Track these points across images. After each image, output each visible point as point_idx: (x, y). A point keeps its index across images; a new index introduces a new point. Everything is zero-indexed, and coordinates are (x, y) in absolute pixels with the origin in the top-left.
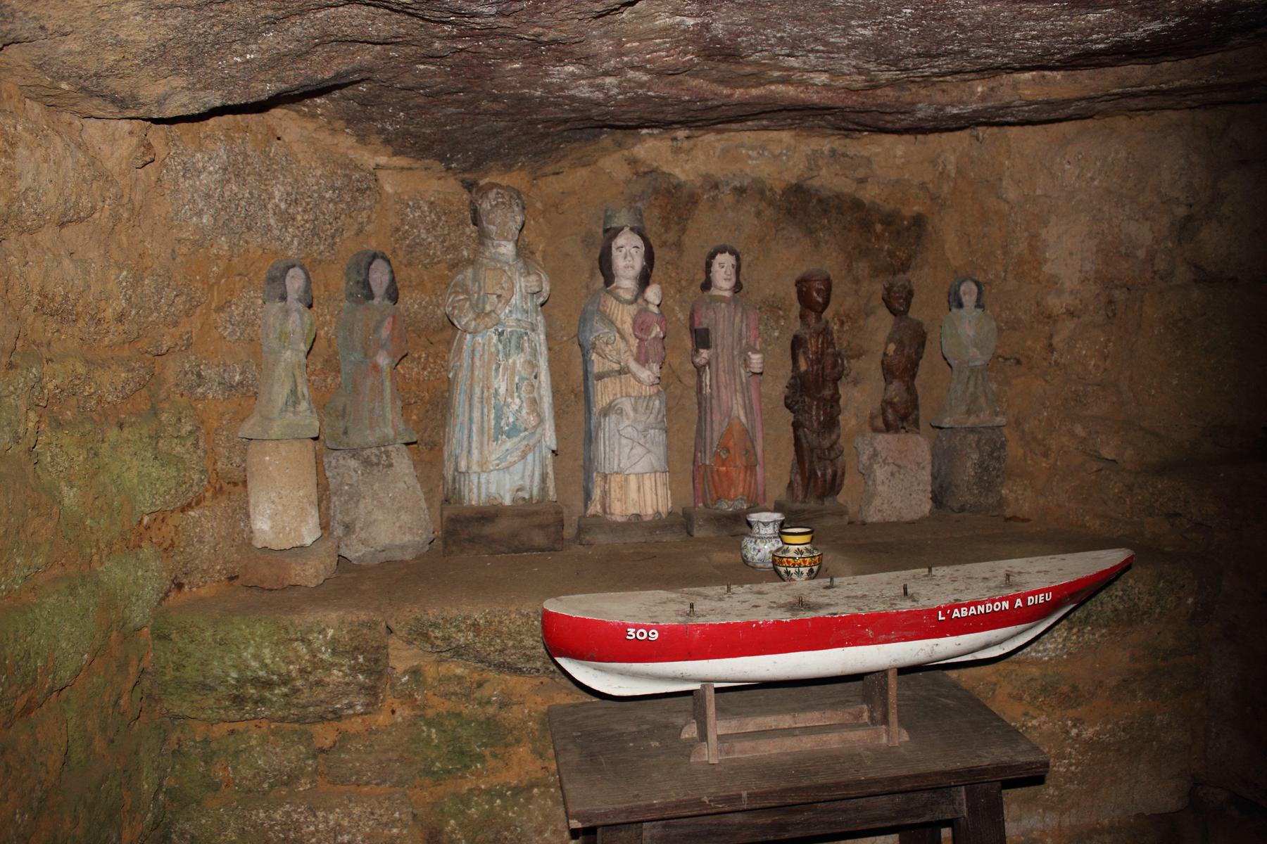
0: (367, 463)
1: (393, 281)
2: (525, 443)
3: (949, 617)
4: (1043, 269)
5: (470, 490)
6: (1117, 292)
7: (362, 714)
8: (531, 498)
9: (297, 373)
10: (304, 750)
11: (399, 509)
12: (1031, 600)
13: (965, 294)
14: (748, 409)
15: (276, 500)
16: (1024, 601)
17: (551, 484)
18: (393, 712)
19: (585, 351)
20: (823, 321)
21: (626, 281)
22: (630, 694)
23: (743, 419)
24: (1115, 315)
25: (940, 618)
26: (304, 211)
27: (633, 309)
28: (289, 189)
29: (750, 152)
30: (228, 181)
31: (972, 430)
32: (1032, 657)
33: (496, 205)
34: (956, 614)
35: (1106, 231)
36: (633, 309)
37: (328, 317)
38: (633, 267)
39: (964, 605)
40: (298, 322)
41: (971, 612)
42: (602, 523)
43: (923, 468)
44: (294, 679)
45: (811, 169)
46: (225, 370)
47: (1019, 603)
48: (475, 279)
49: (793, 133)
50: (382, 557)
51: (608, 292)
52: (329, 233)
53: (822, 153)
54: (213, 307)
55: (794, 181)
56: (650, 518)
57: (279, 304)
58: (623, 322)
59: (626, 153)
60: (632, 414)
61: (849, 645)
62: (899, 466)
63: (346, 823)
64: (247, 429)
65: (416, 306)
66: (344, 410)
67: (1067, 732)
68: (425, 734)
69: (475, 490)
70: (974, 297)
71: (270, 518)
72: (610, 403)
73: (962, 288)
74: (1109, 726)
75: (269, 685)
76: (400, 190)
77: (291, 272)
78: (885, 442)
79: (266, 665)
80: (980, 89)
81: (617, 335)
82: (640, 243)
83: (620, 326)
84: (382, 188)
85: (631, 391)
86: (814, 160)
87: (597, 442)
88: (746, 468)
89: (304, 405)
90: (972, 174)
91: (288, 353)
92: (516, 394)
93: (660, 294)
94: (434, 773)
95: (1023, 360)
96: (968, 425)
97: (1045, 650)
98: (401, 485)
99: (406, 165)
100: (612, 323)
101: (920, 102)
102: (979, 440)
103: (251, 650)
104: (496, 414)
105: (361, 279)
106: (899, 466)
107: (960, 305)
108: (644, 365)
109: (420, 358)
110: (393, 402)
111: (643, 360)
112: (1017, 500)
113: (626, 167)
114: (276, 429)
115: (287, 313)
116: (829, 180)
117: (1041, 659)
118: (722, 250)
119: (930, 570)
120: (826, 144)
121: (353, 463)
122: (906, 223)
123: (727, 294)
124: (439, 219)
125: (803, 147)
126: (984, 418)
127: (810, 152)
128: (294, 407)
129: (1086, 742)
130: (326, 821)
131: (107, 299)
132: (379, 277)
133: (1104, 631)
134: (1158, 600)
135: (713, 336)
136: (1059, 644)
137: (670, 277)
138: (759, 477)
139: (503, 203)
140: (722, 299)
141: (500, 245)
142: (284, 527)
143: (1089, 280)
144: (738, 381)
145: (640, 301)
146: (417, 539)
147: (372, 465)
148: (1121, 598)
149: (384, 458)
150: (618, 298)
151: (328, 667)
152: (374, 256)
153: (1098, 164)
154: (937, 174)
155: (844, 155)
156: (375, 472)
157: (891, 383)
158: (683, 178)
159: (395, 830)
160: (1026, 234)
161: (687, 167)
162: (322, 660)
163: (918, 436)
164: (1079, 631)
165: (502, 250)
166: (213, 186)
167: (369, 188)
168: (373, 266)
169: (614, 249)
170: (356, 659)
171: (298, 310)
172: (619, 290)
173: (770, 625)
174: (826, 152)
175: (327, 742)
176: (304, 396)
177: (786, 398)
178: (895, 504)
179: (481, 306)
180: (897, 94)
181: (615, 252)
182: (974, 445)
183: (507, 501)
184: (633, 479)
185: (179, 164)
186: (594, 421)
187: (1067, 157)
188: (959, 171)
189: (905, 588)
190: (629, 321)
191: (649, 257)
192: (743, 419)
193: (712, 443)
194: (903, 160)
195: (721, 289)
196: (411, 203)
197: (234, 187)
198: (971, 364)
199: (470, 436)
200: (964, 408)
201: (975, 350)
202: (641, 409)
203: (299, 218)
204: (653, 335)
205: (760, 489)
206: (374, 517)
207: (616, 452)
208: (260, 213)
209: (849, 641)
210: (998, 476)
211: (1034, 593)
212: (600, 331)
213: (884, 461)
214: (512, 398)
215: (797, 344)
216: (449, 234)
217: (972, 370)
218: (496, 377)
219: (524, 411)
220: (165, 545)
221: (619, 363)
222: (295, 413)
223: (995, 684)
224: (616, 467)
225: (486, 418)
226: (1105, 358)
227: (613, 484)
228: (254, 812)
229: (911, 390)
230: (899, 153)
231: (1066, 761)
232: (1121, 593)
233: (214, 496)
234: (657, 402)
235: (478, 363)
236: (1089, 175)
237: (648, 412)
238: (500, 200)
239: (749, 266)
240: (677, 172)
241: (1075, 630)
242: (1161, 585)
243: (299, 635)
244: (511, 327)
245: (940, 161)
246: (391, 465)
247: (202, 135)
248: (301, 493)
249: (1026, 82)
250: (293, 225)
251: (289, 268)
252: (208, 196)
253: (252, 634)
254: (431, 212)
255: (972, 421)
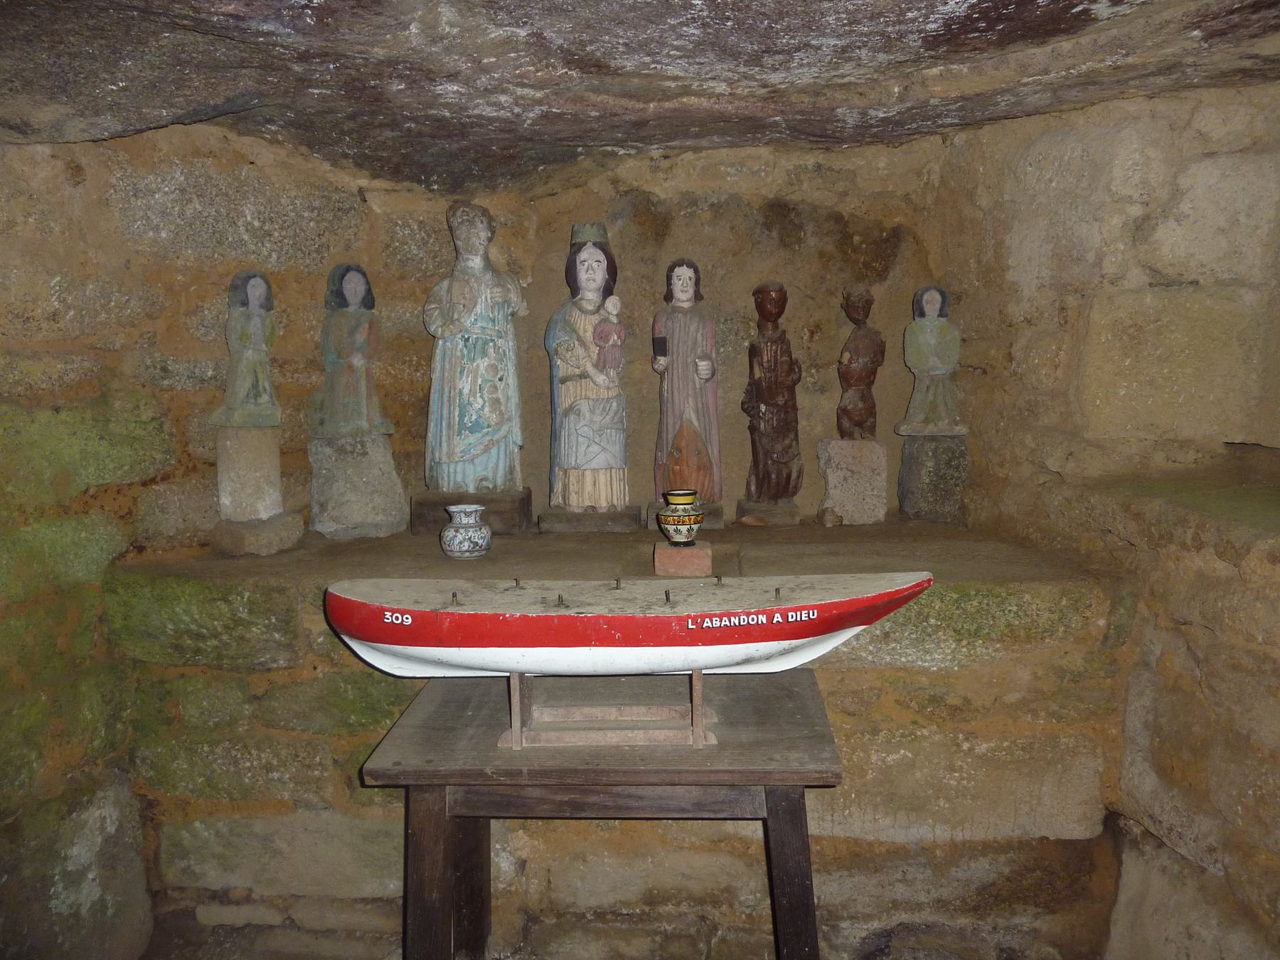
0: (341, 450)
1: (369, 291)
2: (489, 438)
3: (700, 626)
4: (1006, 276)
5: (442, 479)
6: (1071, 298)
7: (286, 668)
8: (495, 487)
9: (259, 370)
10: (241, 696)
11: (373, 493)
12: (792, 617)
13: (927, 303)
14: (702, 412)
15: (235, 479)
16: (785, 617)
17: (518, 475)
18: (315, 668)
19: (550, 356)
20: (780, 330)
21: (590, 295)
22: (391, 672)
23: (696, 423)
24: (1066, 322)
25: (690, 626)
26: (282, 228)
27: (595, 319)
28: (262, 208)
29: (729, 169)
30: (190, 201)
31: (933, 438)
32: (920, 666)
33: (462, 222)
34: (707, 623)
35: (1060, 234)
36: (595, 319)
37: (314, 322)
38: (594, 280)
39: (716, 615)
40: (259, 325)
41: (723, 623)
42: (562, 514)
43: (879, 474)
44: (220, 634)
45: (792, 185)
46: (195, 367)
47: (778, 618)
48: (449, 291)
49: (771, 149)
50: (356, 534)
51: (574, 304)
52: (313, 248)
53: (806, 168)
54: (182, 311)
55: (771, 196)
56: (605, 511)
57: (241, 309)
58: (585, 331)
59: (610, 173)
60: (588, 415)
61: (595, 646)
62: (852, 471)
63: (275, 762)
64: (217, 416)
65: (408, 315)
66: (322, 404)
67: (958, 745)
68: (342, 690)
69: (446, 479)
70: (938, 306)
71: (231, 494)
72: (572, 404)
73: (925, 297)
74: (1005, 744)
75: (199, 637)
76: (389, 211)
77: (252, 282)
78: (838, 448)
79: (196, 620)
80: (896, 90)
81: (576, 343)
82: (602, 257)
83: (582, 334)
84: (371, 209)
85: (589, 394)
86: (796, 176)
87: (560, 440)
88: (699, 468)
89: (265, 398)
90: (953, 183)
91: (250, 352)
92: (478, 395)
93: (619, 306)
94: (351, 725)
95: (988, 369)
96: (926, 433)
97: (933, 660)
98: (376, 472)
99: (388, 188)
100: (575, 331)
101: (838, 107)
102: (937, 447)
103: (183, 606)
104: (460, 411)
105: (335, 289)
106: (852, 471)
107: (922, 315)
108: (602, 372)
109: (411, 361)
110: (369, 396)
111: (601, 366)
112: (976, 510)
113: (610, 187)
114: (237, 417)
115: (248, 317)
116: (810, 193)
117: (929, 668)
118: (680, 263)
119: (719, 579)
120: (810, 160)
121: (328, 450)
122: (885, 234)
123: (686, 305)
124: (429, 236)
125: (783, 162)
126: (942, 427)
127: (792, 167)
128: (256, 399)
129: (979, 757)
130: (259, 759)
131: (35, 301)
132: (354, 287)
133: (998, 646)
134: (1060, 619)
135: (669, 345)
136: (947, 655)
137: (645, 290)
138: (716, 478)
139: (468, 221)
140: (684, 312)
141: (468, 259)
142: (242, 502)
143: (1045, 286)
144: (691, 385)
145: (602, 311)
146: (391, 519)
147: (346, 452)
148: (1016, 613)
149: (359, 447)
150: (581, 310)
151: (247, 624)
152: (348, 269)
153: (1056, 164)
154: (922, 184)
155: (830, 169)
156: (349, 459)
157: (847, 391)
158: (663, 196)
159: (316, 772)
160: (993, 241)
161: (666, 185)
162: (241, 618)
163: (874, 443)
164: (969, 644)
165: (471, 264)
166: (170, 205)
167: (352, 208)
168: (346, 278)
169: (578, 263)
170: (269, 619)
171: (260, 316)
172: (584, 302)
173: (517, 619)
174: (810, 167)
175: (261, 690)
176: (265, 390)
177: (743, 403)
178: (846, 508)
179: (451, 314)
180: (812, 100)
181: (579, 266)
182: (931, 454)
183: (471, 490)
184: (588, 473)
185: (129, 185)
186: (558, 420)
187: (1029, 159)
188: (943, 181)
189: (667, 594)
190: (590, 329)
191: (612, 270)
192: (696, 423)
193: (667, 443)
194: (886, 172)
195: (679, 300)
196: (400, 222)
197: (197, 206)
198: (932, 373)
199: (441, 431)
200: (922, 417)
201: (936, 359)
202: (598, 411)
203: (276, 234)
204: (610, 343)
205: (716, 489)
206: (346, 498)
207: (574, 449)
208: (230, 230)
209: (596, 641)
210: (957, 485)
211: (795, 610)
212: (560, 338)
213: (837, 466)
214: (475, 397)
215: (754, 352)
216: (440, 250)
217: (932, 379)
218: (460, 379)
219: (487, 409)
220: (121, 513)
221: (579, 368)
222: (256, 404)
223: (881, 690)
224: (573, 463)
225: (452, 416)
226: (1056, 367)
227: (571, 479)
228: (200, 746)
229: (867, 397)
230: (881, 165)
231: (957, 775)
232: (1015, 608)
233: (185, 474)
234: (615, 404)
235: (447, 366)
236: (1048, 176)
237: (605, 413)
238: (465, 218)
239: (722, 278)
240: (657, 190)
241: (964, 642)
242: (1064, 602)
243: (220, 595)
244: (476, 334)
245: (925, 171)
246: (366, 453)
247: (155, 160)
248: (258, 474)
249: (934, 78)
250: (270, 241)
251: (250, 278)
252: (164, 213)
253: (183, 592)
254: (420, 230)
255: (930, 429)
